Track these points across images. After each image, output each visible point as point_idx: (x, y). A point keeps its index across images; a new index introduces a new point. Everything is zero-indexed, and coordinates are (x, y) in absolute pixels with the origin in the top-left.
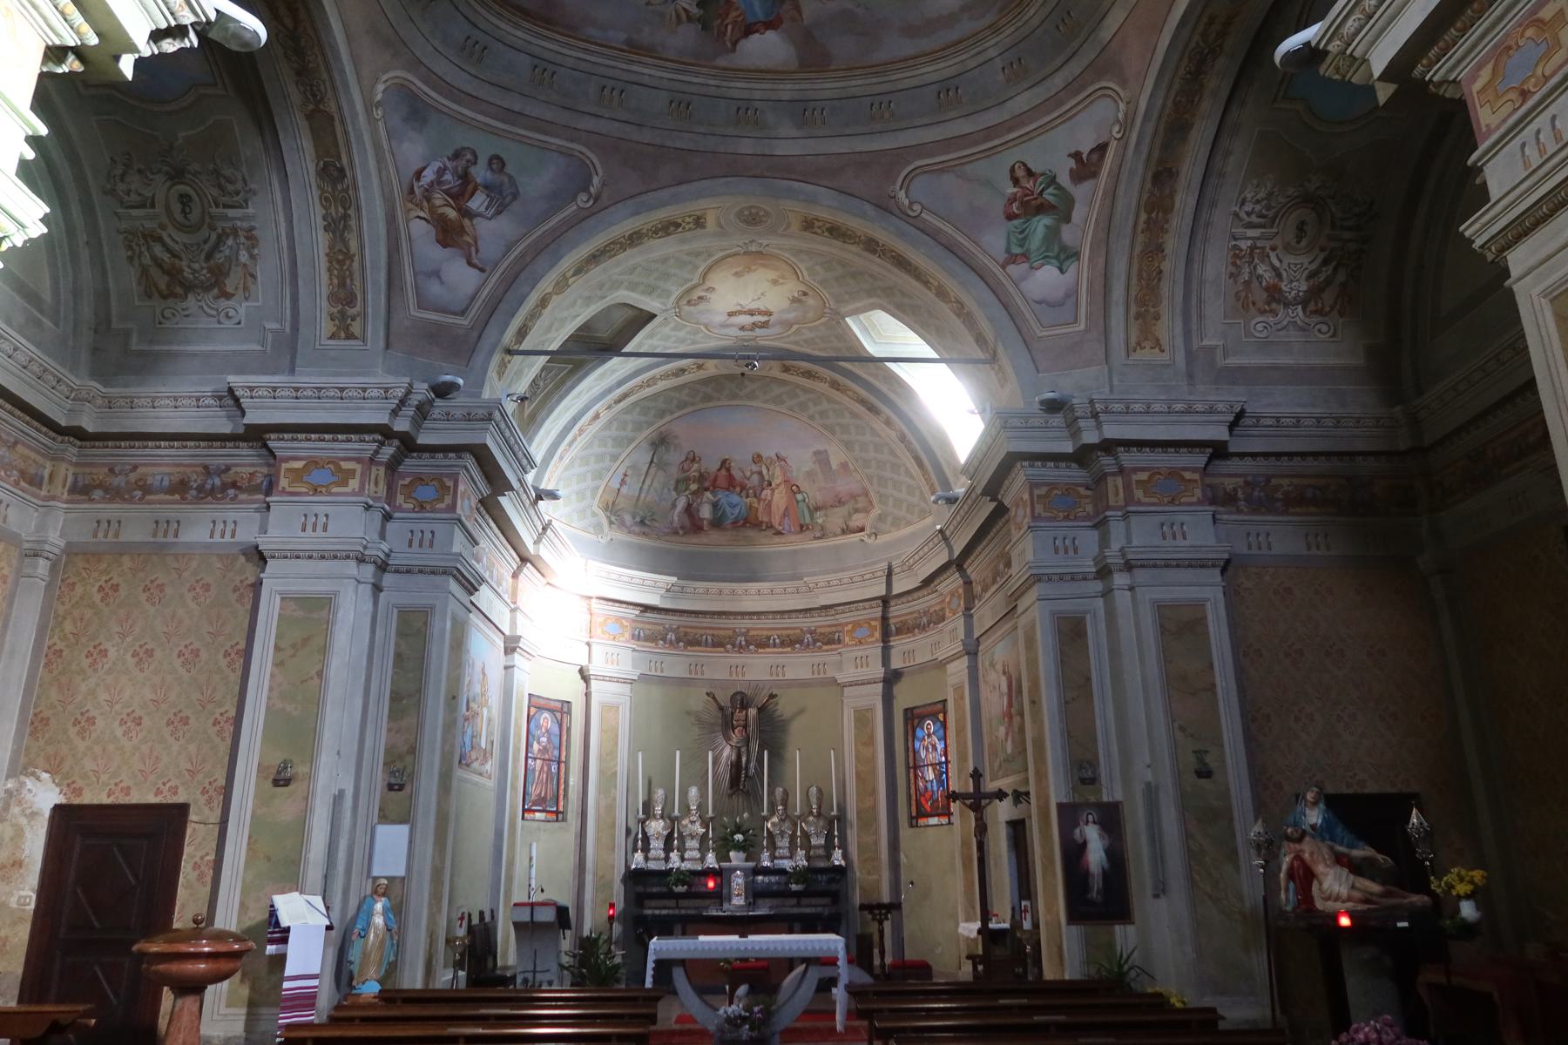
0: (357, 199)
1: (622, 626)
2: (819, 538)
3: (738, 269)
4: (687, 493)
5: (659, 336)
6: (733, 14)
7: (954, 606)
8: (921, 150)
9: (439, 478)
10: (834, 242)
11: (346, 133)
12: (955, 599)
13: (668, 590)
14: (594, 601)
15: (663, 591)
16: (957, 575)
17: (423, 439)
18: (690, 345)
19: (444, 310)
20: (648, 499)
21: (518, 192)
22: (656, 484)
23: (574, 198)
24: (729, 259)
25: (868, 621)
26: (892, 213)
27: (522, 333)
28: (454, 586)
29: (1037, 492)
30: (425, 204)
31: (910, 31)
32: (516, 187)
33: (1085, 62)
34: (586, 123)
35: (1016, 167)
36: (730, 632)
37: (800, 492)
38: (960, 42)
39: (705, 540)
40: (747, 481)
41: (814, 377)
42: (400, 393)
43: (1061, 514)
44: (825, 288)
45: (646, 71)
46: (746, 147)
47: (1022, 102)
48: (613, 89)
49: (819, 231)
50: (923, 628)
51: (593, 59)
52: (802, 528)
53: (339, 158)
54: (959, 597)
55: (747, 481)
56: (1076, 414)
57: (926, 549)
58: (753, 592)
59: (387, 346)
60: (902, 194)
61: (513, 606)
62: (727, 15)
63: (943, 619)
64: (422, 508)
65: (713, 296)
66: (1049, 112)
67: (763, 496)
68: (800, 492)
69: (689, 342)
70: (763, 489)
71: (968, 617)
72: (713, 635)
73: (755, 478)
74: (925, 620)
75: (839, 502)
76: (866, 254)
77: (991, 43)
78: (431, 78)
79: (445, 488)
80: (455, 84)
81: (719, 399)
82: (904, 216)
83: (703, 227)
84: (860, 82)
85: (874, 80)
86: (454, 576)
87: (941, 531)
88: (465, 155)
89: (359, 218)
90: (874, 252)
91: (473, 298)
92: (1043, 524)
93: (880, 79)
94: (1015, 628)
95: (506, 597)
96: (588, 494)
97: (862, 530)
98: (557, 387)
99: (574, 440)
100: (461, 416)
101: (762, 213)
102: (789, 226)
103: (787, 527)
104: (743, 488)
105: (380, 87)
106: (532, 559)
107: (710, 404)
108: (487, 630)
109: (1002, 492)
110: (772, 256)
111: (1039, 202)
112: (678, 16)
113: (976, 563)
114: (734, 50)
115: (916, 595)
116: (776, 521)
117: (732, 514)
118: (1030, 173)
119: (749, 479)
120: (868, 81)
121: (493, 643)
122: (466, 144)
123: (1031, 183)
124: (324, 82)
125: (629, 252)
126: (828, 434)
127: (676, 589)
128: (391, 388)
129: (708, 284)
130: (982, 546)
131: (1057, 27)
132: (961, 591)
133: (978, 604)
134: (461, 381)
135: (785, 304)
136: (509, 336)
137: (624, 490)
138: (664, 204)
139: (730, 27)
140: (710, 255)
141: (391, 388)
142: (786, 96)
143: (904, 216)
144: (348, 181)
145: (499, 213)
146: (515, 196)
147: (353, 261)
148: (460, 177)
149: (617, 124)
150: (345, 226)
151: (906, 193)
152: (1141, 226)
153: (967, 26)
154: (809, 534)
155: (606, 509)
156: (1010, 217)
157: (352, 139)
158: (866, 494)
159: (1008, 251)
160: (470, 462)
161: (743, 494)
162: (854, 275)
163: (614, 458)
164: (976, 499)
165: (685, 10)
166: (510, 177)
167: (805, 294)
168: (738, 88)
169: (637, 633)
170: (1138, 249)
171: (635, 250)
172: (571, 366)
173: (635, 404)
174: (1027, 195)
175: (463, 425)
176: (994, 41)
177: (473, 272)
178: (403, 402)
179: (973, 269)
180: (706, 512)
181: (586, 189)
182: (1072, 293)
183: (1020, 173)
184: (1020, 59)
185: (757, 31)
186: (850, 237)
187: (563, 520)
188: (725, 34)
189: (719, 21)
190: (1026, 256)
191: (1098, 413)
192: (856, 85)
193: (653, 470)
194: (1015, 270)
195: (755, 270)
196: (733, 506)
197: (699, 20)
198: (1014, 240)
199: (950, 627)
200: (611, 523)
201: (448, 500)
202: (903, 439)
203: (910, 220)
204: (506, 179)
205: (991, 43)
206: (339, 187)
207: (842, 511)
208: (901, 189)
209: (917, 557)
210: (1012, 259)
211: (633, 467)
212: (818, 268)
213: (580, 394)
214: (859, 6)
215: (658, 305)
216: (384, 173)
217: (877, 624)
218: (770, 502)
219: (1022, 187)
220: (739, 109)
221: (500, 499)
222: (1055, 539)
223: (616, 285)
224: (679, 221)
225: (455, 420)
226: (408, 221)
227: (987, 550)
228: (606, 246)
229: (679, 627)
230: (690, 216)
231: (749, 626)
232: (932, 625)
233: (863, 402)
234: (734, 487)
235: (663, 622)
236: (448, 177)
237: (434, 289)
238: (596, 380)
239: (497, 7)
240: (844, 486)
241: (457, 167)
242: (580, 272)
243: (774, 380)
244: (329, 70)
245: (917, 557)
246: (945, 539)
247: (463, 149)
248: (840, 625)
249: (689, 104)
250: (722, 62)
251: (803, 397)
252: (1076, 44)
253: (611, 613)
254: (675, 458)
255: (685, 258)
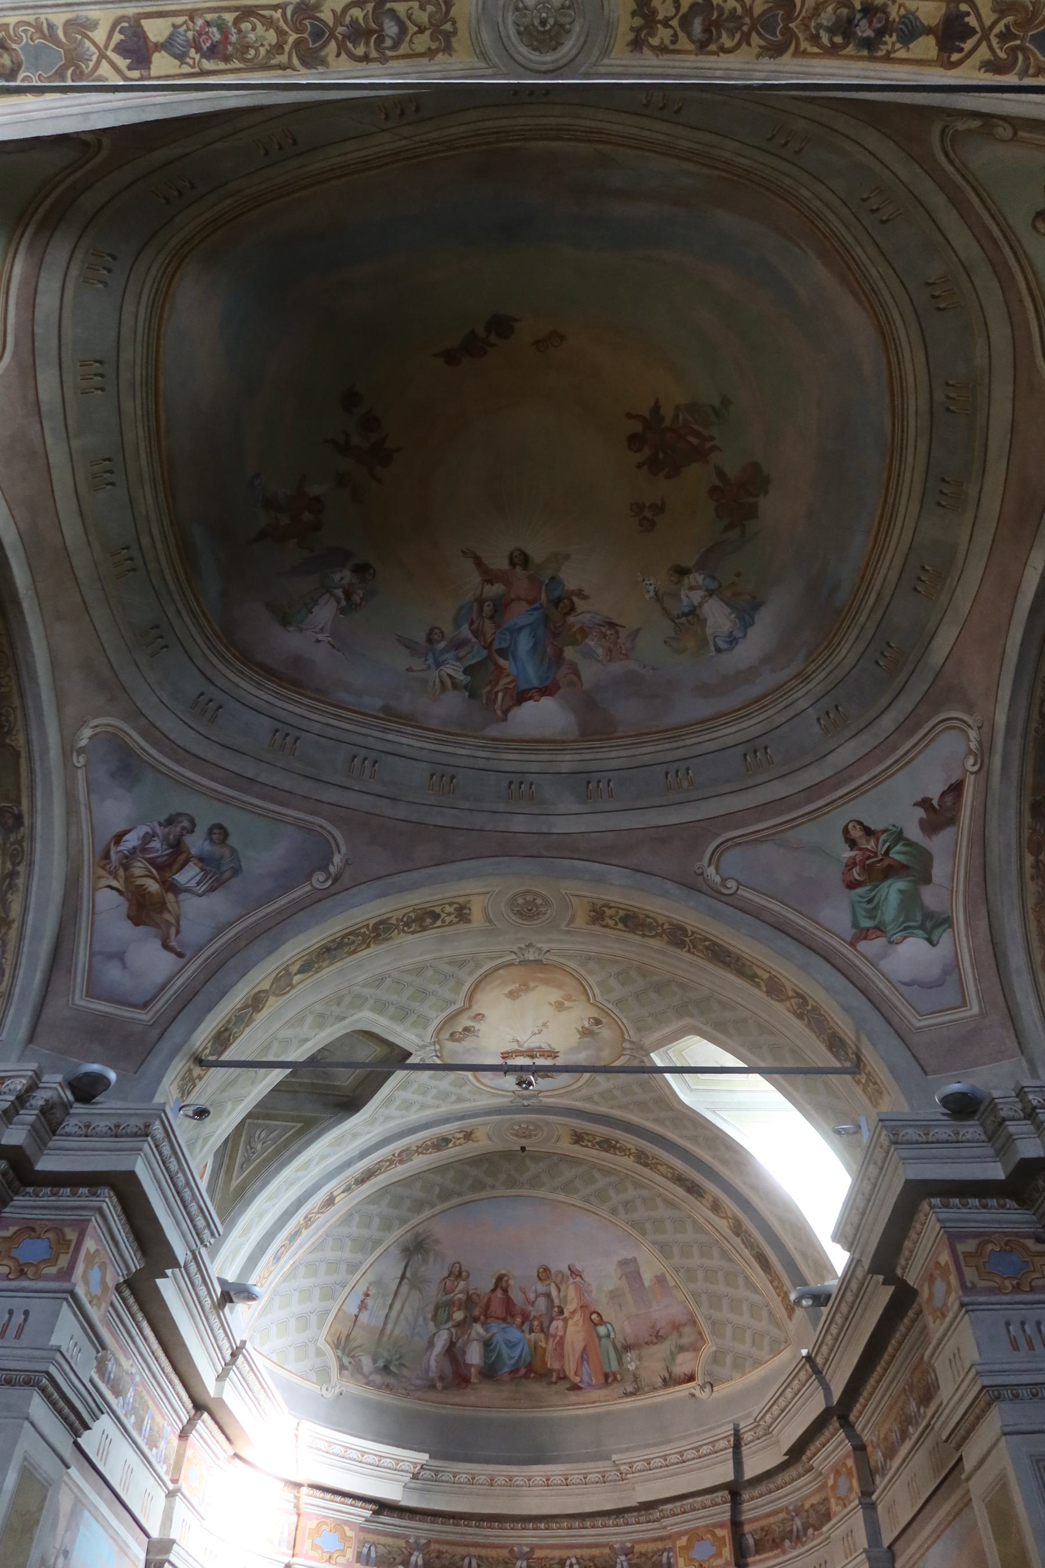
0: (32, 851)
1: (344, 1538)
2: (632, 1394)
3: (512, 987)
4: (450, 1324)
5: (415, 1087)
6: (505, 681)
7: (842, 1491)
8: (730, 819)
9: (58, 1229)
10: (631, 937)
11: (31, 771)
12: (842, 1479)
13: (415, 1477)
14: (305, 1490)
15: (407, 1478)
16: (841, 1434)
17: (46, 1164)
18: (453, 1103)
19: (123, 1002)
20: (396, 1332)
21: (240, 866)
22: (407, 1310)
23: (309, 877)
24: (501, 971)
25: (710, 1529)
26: (699, 891)
27: (223, 1038)
28: (38, 1408)
29: (961, 1248)
30: (121, 872)
31: (705, 690)
32: (239, 861)
33: (917, 697)
34: (332, 795)
35: (850, 826)
36: (505, 1553)
37: (602, 1322)
38: (764, 696)
39: (472, 1399)
40: (530, 1308)
41: (614, 1147)
42: (19, 1085)
43: (1007, 1283)
44: (621, 1011)
45: (406, 741)
46: (520, 824)
47: (845, 754)
48: (365, 759)
49: (611, 923)
50: (798, 1539)
51: (345, 726)
52: (608, 1379)
53: (19, 802)
54: (849, 1474)
55: (530, 1308)
56: (1002, 1114)
57: (789, 1393)
58: (538, 1480)
59: (31, 1038)
60: (711, 870)
61: (171, 1486)
62: (497, 682)
63: (828, 1516)
64: (22, 1273)
65: (482, 1027)
66: (880, 761)
67: (552, 1330)
68: (602, 1322)
69: (454, 1098)
70: (552, 1319)
71: (869, 1507)
72: (480, 1558)
73: (542, 1302)
74: (798, 1523)
75: (657, 1336)
76: (671, 950)
77: (799, 694)
78: (152, 733)
79: (63, 1243)
80: (179, 742)
81: (493, 1187)
82: (716, 894)
83: (469, 921)
84: (653, 749)
85: (667, 746)
86: (43, 1390)
87: (809, 1358)
88: (181, 822)
89: (29, 875)
90: (681, 945)
91: (163, 987)
92: (982, 1299)
93: (675, 745)
94: (967, 1503)
95: (162, 1470)
96: (314, 1320)
97: (691, 1378)
98: (278, 1152)
99: (296, 1234)
100: (105, 1130)
101: (539, 901)
102: (572, 920)
103: (586, 1378)
104: (526, 1317)
105: (87, 733)
106: (212, 1406)
107: (482, 1195)
108: (114, 1522)
109: (903, 1262)
110: (560, 968)
111: (886, 862)
112: (442, 682)
113: (869, 1410)
114: (505, 719)
115: (779, 1480)
116: (570, 1369)
117: (510, 1357)
118: (868, 832)
119: (533, 1304)
120: (659, 748)
121: (124, 1550)
122: (183, 810)
123: (872, 843)
124: (14, 709)
125: (373, 948)
126: (635, 1234)
127: (426, 1474)
128: (9, 1077)
129: (476, 1009)
130: (876, 1375)
131: (877, 662)
132: (850, 1463)
133: (880, 1482)
134: (112, 1076)
135: (574, 1039)
136: (202, 1037)
137: (364, 1317)
138: (417, 885)
139: (500, 695)
140: (478, 966)
141: (9, 1077)
142: (565, 768)
143: (716, 894)
144: (24, 830)
145: (212, 889)
146: (236, 871)
147: (10, 928)
148: (171, 846)
149: (367, 797)
150: (10, 886)
151: (717, 869)
152: (1029, 871)
153: (766, 681)
154: (617, 1389)
155: (336, 1346)
156: (852, 885)
157: (38, 779)
158: (694, 1323)
159: (855, 924)
160: (108, 1203)
161: (526, 1327)
162: (660, 988)
163: (352, 1268)
164: (865, 1278)
165: (449, 675)
166: (233, 851)
167: (598, 1022)
168: (510, 760)
169: (365, 1550)
170: (1031, 902)
171: (385, 946)
172: (299, 1125)
173: (384, 1191)
174: (869, 858)
175: (108, 1143)
176: (804, 691)
177: (170, 957)
178: (22, 1100)
179: (814, 951)
180: (474, 1356)
181: (324, 868)
182: (953, 967)
183: (856, 833)
184: (837, 707)
185: (531, 698)
186: (650, 927)
187: (275, 1358)
188: (495, 701)
189: (488, 688)
190: (880, 929)
191: (1034, 1108)
192: (647, 752)
193: (404, 1289)
194: (870, 947)
195: (534, 988)
196: (511, 1345)
197: (466, 687)
198: (861, 912)
199: (843, 1529)
200: (342, 1367)
201: (63, 1261)
202: (738, 1228)
203: (723, 898)
204: (227, 853)
205: (799, 694)
206: (12, 838)
207: (661, 1350)
208: (709, 865)
209: (776, 1410)
210: (863, 934)
211: (378, 1283)
212: (612, 982)
213: (308, 1163)
214: (645, 667)
215: (413, 1038)
216: (74, 829)
217: (724, 1533)
218: (562, 1338)
219: (861, 849)
220: (511, 783)
221: (160, 1282)
222: (1008, 1324)
223: (359, 1002)
224: (438, 910)
225: (97, 1135)
226: (95, 889)
227: (883, 1385)
228: (344, 937)
229: (429, 1542)
230: (451, 904)
231: (535, 1541)
232: (810, 1531)
233: (679, 1179)
234: (513, 1316)
235: (406, 1532)
236: (156, 844)
237: (113, 973)
238: (331, 1145)
239: (239, 665)
240: (663, 1311)
241: (168, 834)
242: (309, 970)
243: (564, 1158)
244: (22, 695)
245: (776, 1410)
246: (817, 1372)
247: (179, 814)
248: (669, 1537)
249: (453, 777)
250: (492, 731)
251: (602, 1182)
252: (902, 678)
253: (331, 1514)
254: (435, 1272)
255: (448, 969)
